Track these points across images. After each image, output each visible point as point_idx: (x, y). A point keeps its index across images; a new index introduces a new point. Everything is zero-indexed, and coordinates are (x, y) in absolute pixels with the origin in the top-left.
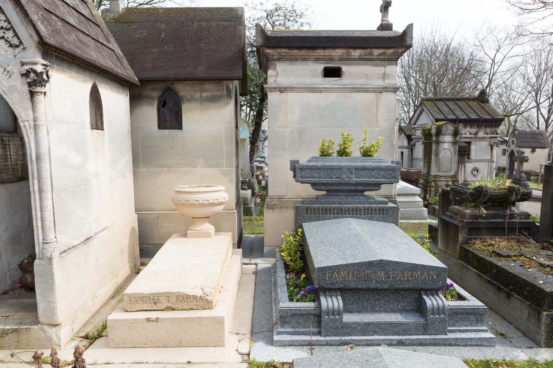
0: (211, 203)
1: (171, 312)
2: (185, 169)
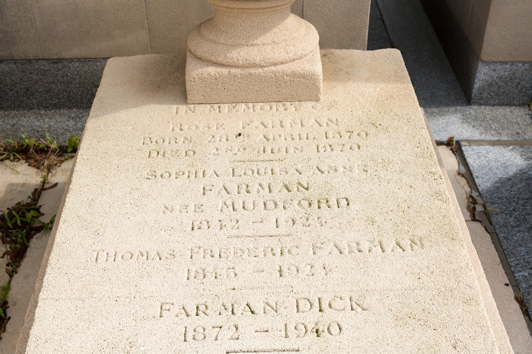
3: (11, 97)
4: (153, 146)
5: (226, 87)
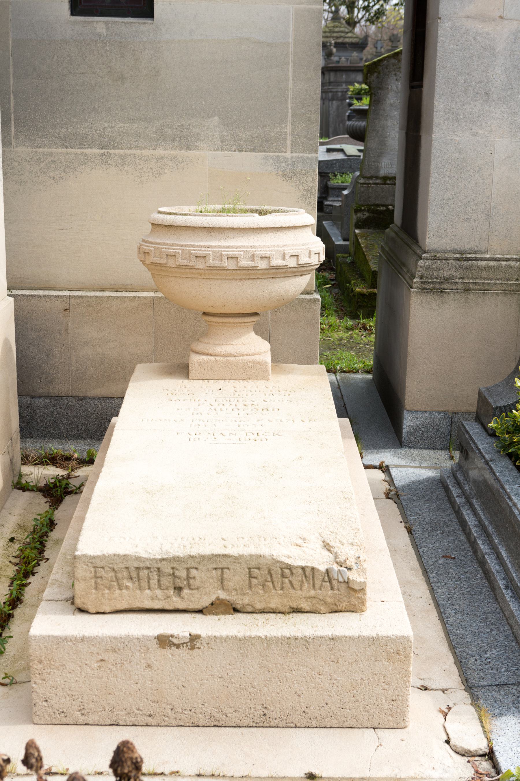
0: (277, 268)
1: (229, 617)
2: (160, 152)
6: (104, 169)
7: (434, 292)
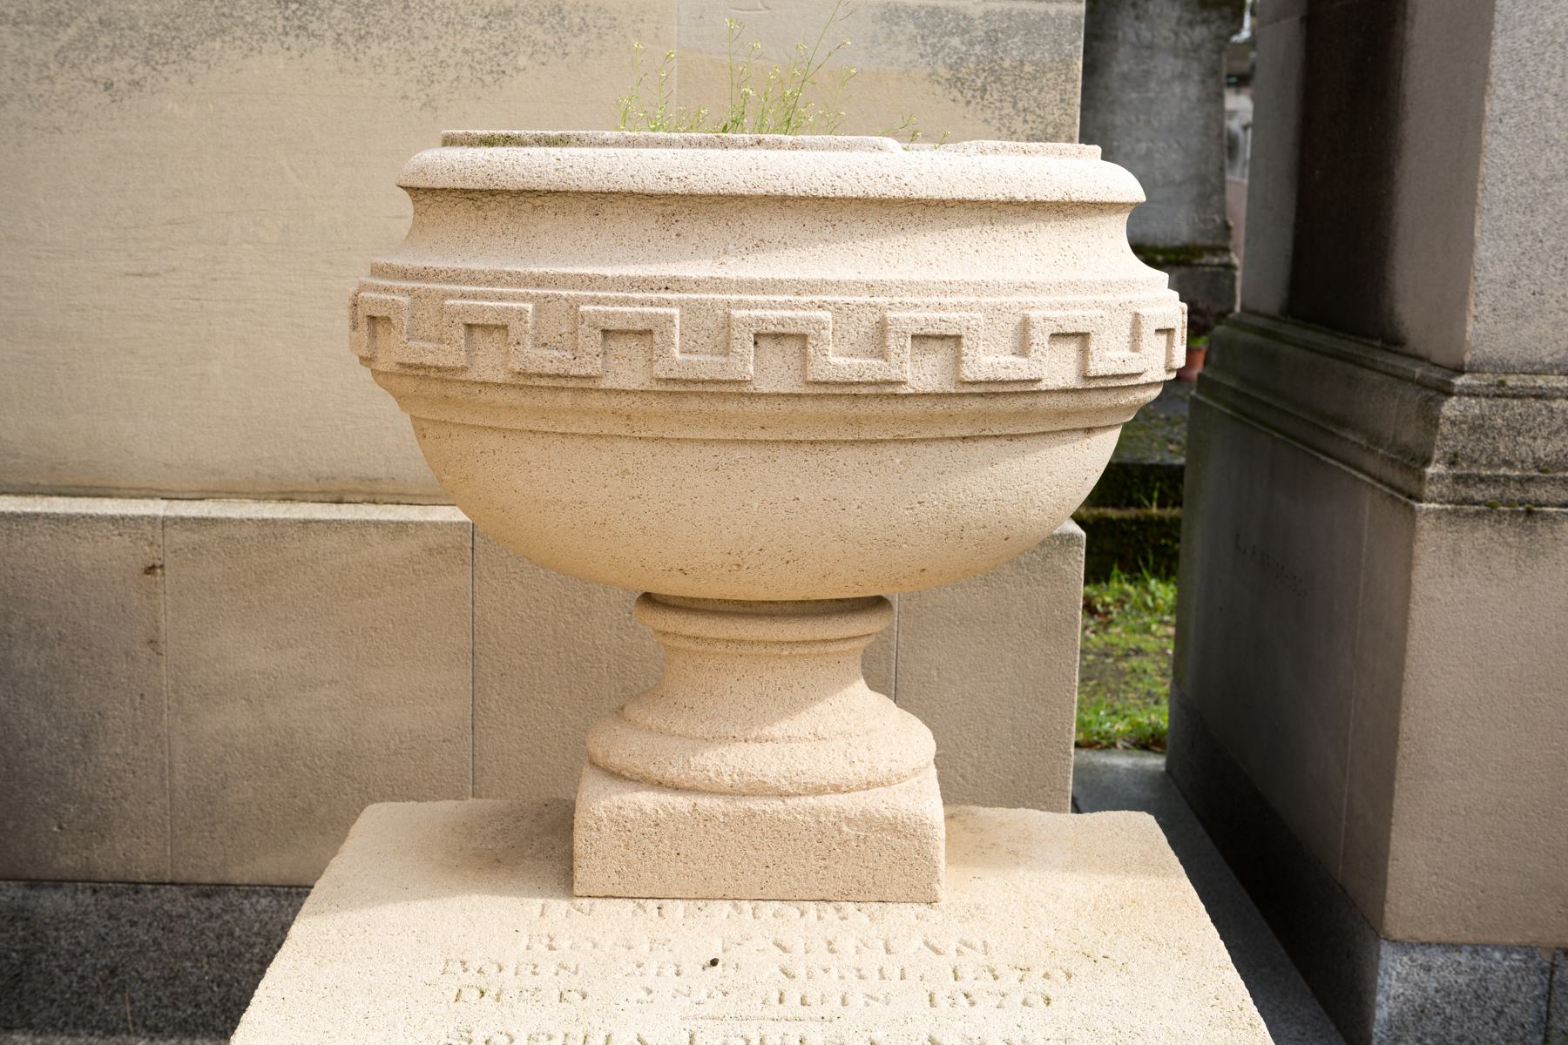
0: (994, 390)
3: (63, 992)
4: (471, 977)
5: (683, 851)
6: (294, 53)
7: (1500, 514)
